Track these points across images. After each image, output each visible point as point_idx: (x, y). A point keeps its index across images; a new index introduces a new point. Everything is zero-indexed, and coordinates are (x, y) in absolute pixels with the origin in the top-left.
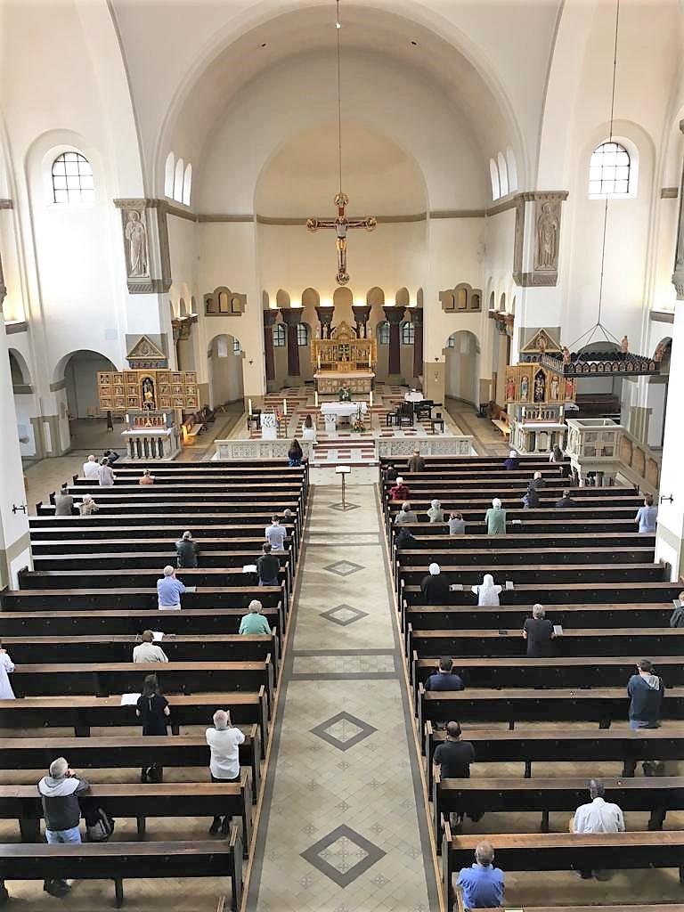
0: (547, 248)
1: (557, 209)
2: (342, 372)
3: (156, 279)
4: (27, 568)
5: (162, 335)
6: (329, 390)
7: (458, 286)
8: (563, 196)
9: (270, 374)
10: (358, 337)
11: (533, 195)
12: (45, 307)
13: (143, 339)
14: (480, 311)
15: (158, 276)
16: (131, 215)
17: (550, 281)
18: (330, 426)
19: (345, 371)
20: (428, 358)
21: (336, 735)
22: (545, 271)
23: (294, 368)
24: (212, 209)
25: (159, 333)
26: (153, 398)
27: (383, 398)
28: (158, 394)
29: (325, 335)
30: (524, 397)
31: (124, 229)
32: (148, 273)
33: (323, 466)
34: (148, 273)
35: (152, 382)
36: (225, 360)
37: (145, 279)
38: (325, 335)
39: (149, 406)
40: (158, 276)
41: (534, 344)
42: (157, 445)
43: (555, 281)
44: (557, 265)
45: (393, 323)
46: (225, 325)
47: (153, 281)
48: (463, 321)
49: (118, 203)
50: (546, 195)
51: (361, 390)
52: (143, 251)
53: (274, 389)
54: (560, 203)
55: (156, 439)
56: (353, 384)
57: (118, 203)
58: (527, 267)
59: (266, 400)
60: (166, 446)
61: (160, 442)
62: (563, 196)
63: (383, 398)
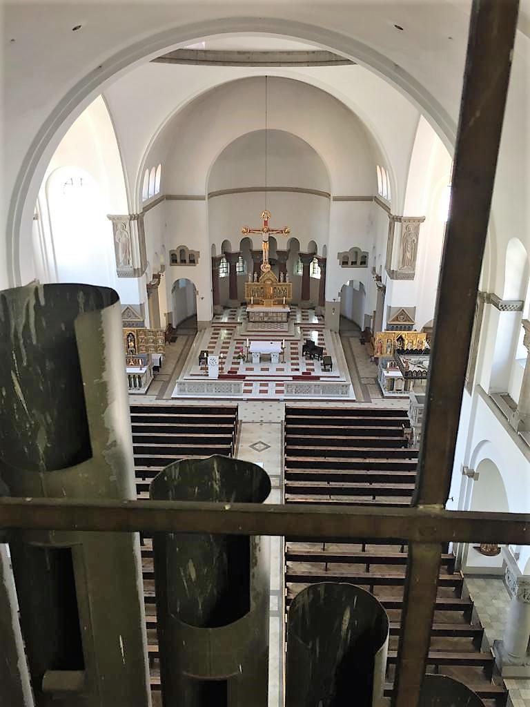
0: (408, 255)
1: (417, 228)
2: (266, 306)
3: (136, 268)
4: (47, 446)
5: (141, 304)
6: (257, 319)
7: (351, 249)
8: (422, 220)
9: (216, 301)
10: (279, 281)
11: (400, 219)
12: (58, 266)
13: (128, 308)
14: (367, 267)
15: (138, 265)
16: (119, 226)
17: (410, 277)
18: (256, 360)
19: (270, 306)
20: (329, 298)
21: (262, 445)
22: (406, 270)
23: (233, 293)
24: (171, 193)
25: (139, 304)
26: (134, 347)
27: (295, 324)
28: (138, 343)
30: (388, 353)
31: (115, 234)
32: (131, 265)
33: (248, 400)
34: (131, 265)
35: (133, 336)
36: (183, 292)
37: (129, 269)
38: (256, 279)
39: (132, 351)
40: (138, 265)
41: (397, 319)
42: (137, 379)
43: (413, 277)
44: (415, 266)
45: (305, 265)
46: (181, 272)
47: (134, 269)
48: (353, 274)
49: (110, 217)
50: (410, 220)
51: (280, 319)
52: (127, 250)
53: (219, 312)
54: (419, 225)
55: (137, 376)
56: (274, 315)
57: (110, 217)
58: (394, 267)
59: (213, 323)
60: (143, 380)
61: (139, 378)
62: (422, 220)
63: (295, 324)
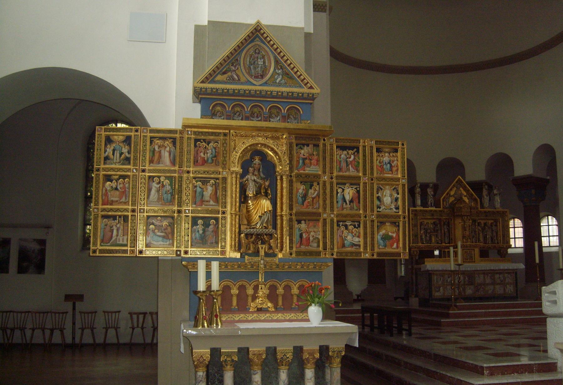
10: (482, 207)
29: (430, 200)
